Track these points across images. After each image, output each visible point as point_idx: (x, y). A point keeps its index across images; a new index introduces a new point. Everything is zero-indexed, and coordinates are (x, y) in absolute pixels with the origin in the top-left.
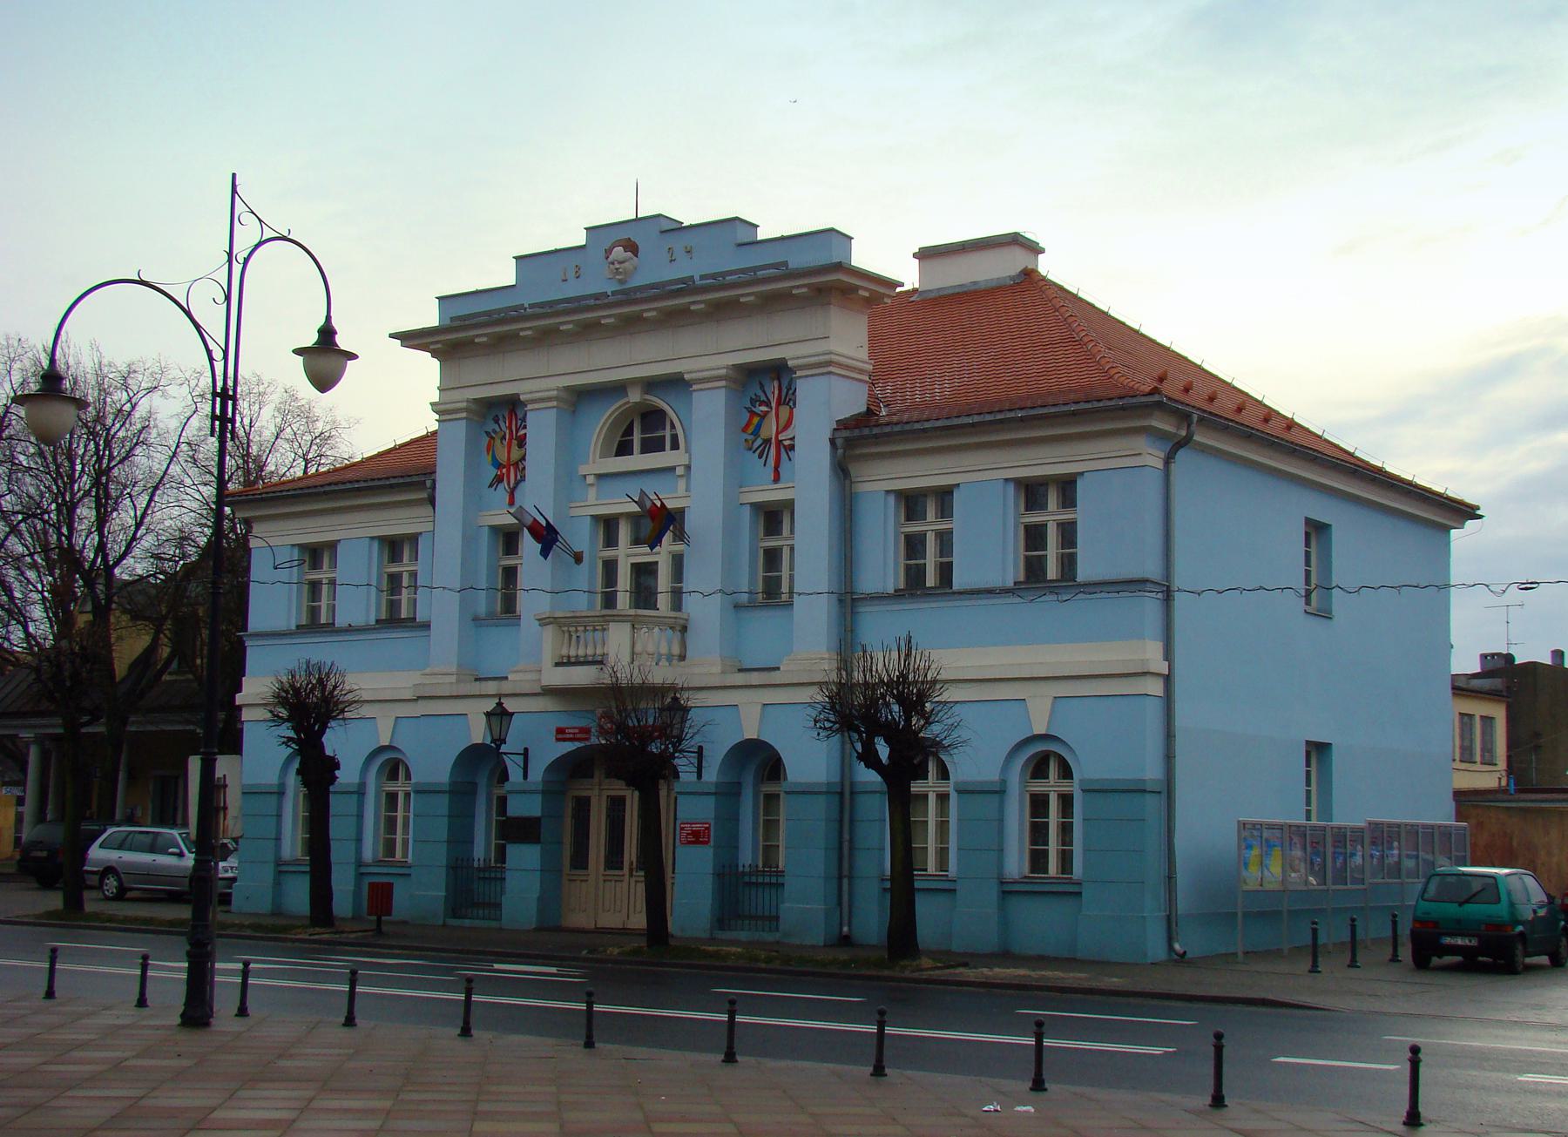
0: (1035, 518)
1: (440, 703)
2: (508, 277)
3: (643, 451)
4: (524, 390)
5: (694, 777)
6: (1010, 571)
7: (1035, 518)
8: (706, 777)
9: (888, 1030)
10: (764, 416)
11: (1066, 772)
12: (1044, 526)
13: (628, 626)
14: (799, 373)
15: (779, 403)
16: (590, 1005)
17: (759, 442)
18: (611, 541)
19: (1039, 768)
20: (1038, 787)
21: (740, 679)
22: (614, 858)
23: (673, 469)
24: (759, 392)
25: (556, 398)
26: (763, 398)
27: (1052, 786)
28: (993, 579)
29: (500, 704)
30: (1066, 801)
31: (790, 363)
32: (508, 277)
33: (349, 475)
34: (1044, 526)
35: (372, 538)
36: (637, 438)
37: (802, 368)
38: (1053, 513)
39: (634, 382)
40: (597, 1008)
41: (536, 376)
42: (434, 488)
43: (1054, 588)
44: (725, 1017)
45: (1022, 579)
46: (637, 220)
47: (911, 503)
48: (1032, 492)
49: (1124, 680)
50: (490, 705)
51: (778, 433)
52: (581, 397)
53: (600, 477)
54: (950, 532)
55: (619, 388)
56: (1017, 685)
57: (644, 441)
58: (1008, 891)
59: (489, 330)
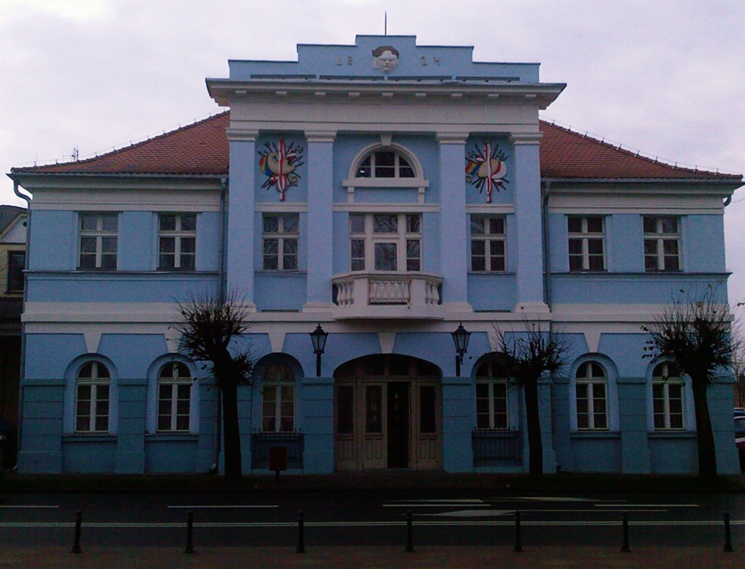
0: (167, 234)
1: (70, 326)
2: (293, 56)
3: (377, 176)
4: (440, 130)
5: (314, 375)
6: (151, 260)
7: (167, 234)
8: (462, 374)
9: (194, 525)
10: (480, 163)
11: (103, 372)
12: (173, 239)
13: (366, 280)
14: (309, 140)
15: (491, 158)
16: (190, 526)
17: (476, 178)
18: (361, 229)
19: (85, 372)
20: (166, 381)
21: (267, 316)
22: (373, 426)
23: (415, 189)
24: (475, 150)
25: (255, 136)
26: (478, 154)
27: (94, 381)
28: (65, 267)
29: (319, 327)
30: (103, 391)
31: (306, 133)
32: (293, 56)
33: (59, 169)
34: (173, 239)
35: (75, 211)
36: (373, 168)
37: (313, 136)
38: (281, 234)
39: (386, 134)
40: (306, 524)
41: (318, 122)
42: (227, 183)
43: (100, 272)
44: (185, 525)
45: (79, 266)
46: (385, 36)
47: (574, 222)
48: (650, 223)
49: (54, 325)
50: (313, 329)
51: (492, 175)
52: (343, 138)
53: (356, 188)
54: (193, 240)
55: (376, 136)
56: (80, 326)
57: (377, 170)
58: (66, 441)
59: (288, 88)
